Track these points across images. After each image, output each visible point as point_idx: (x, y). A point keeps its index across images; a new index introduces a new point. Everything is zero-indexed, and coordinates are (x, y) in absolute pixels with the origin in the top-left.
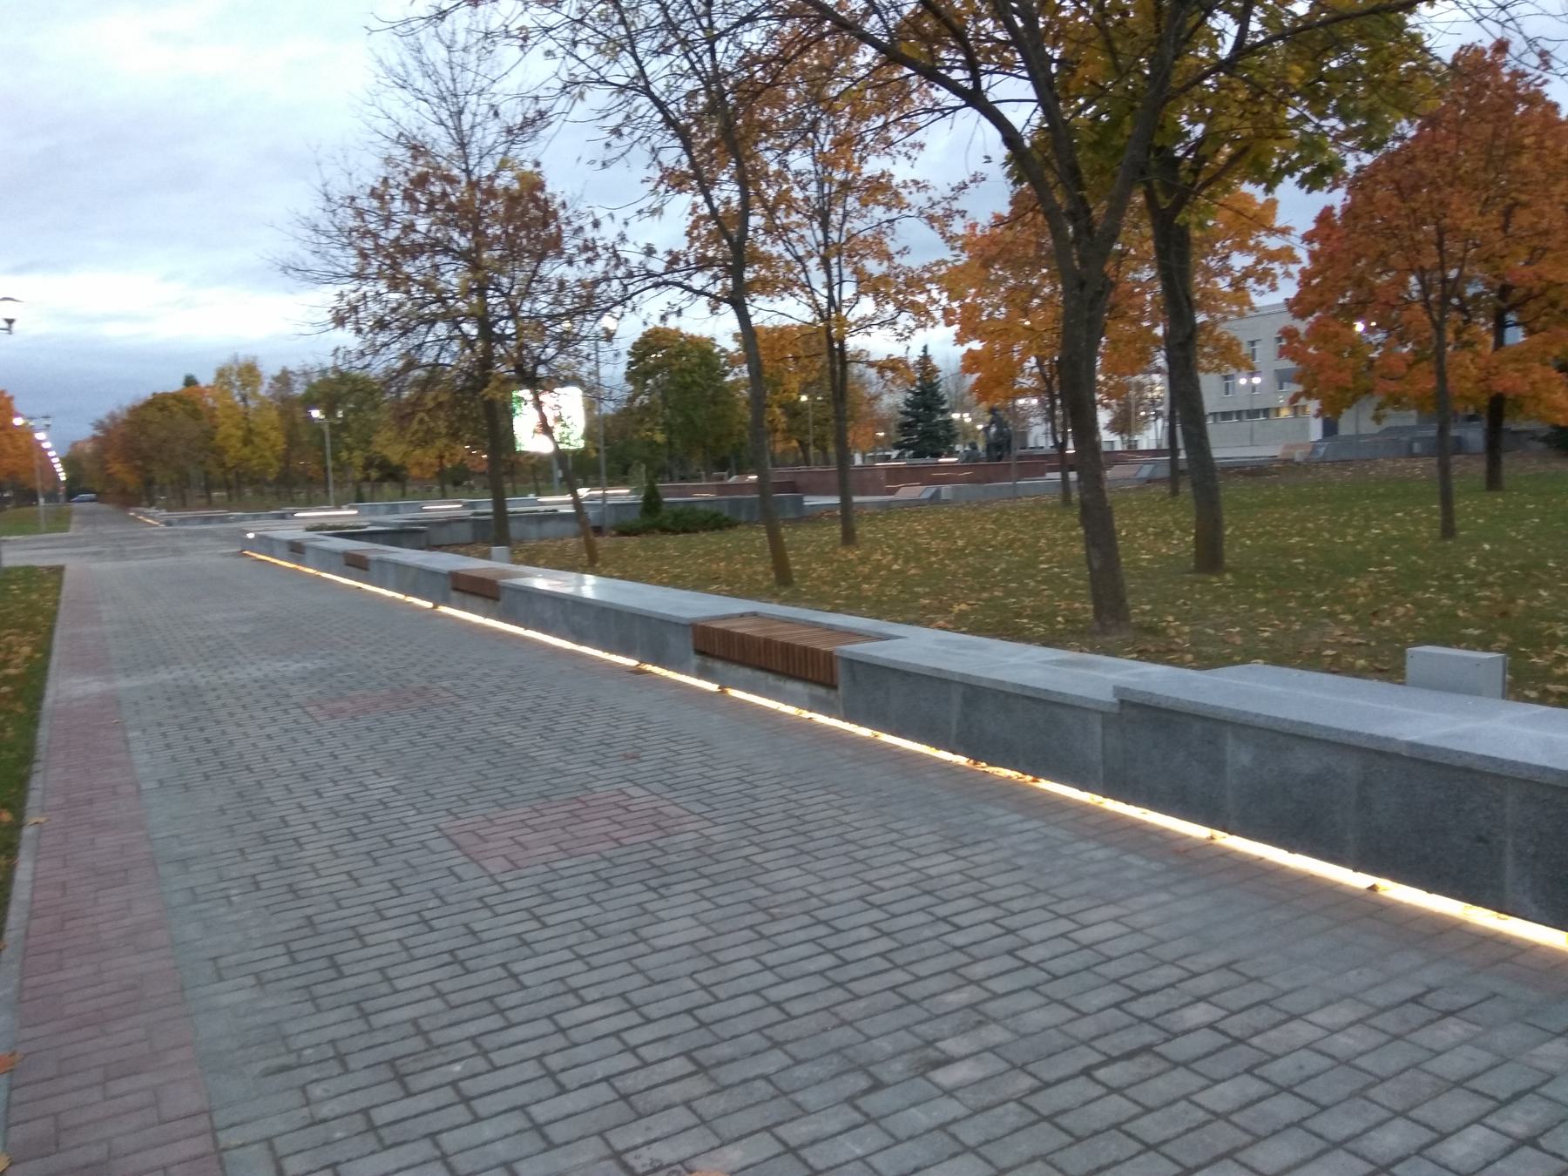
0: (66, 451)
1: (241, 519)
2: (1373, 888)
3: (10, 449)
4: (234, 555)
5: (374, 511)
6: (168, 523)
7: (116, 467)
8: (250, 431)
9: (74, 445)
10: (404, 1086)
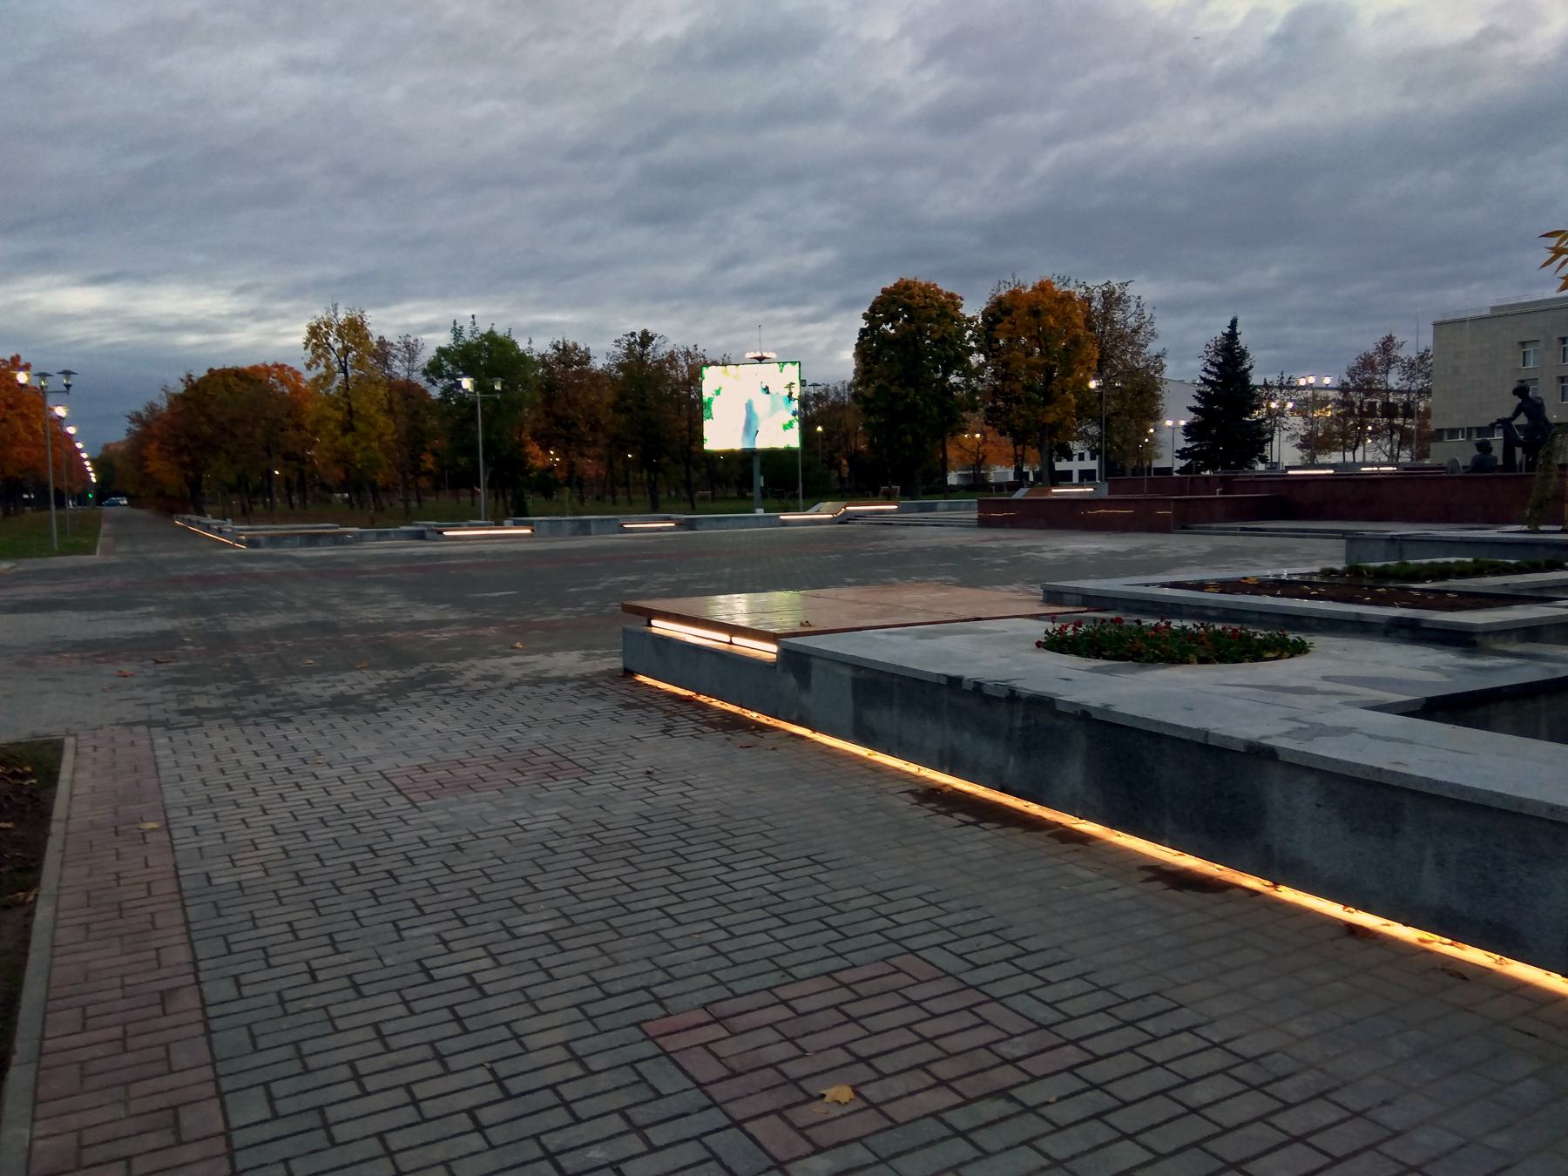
0: (98, 452)
1: (360, 538)
2: (1276, 885)
3: (23, 434)
4: (587, 683)
5: (555, 530)
6: (252, 543)
7: (156, 465)
8: (350, 412)
9: (106, 447)
10: (444, 1065)
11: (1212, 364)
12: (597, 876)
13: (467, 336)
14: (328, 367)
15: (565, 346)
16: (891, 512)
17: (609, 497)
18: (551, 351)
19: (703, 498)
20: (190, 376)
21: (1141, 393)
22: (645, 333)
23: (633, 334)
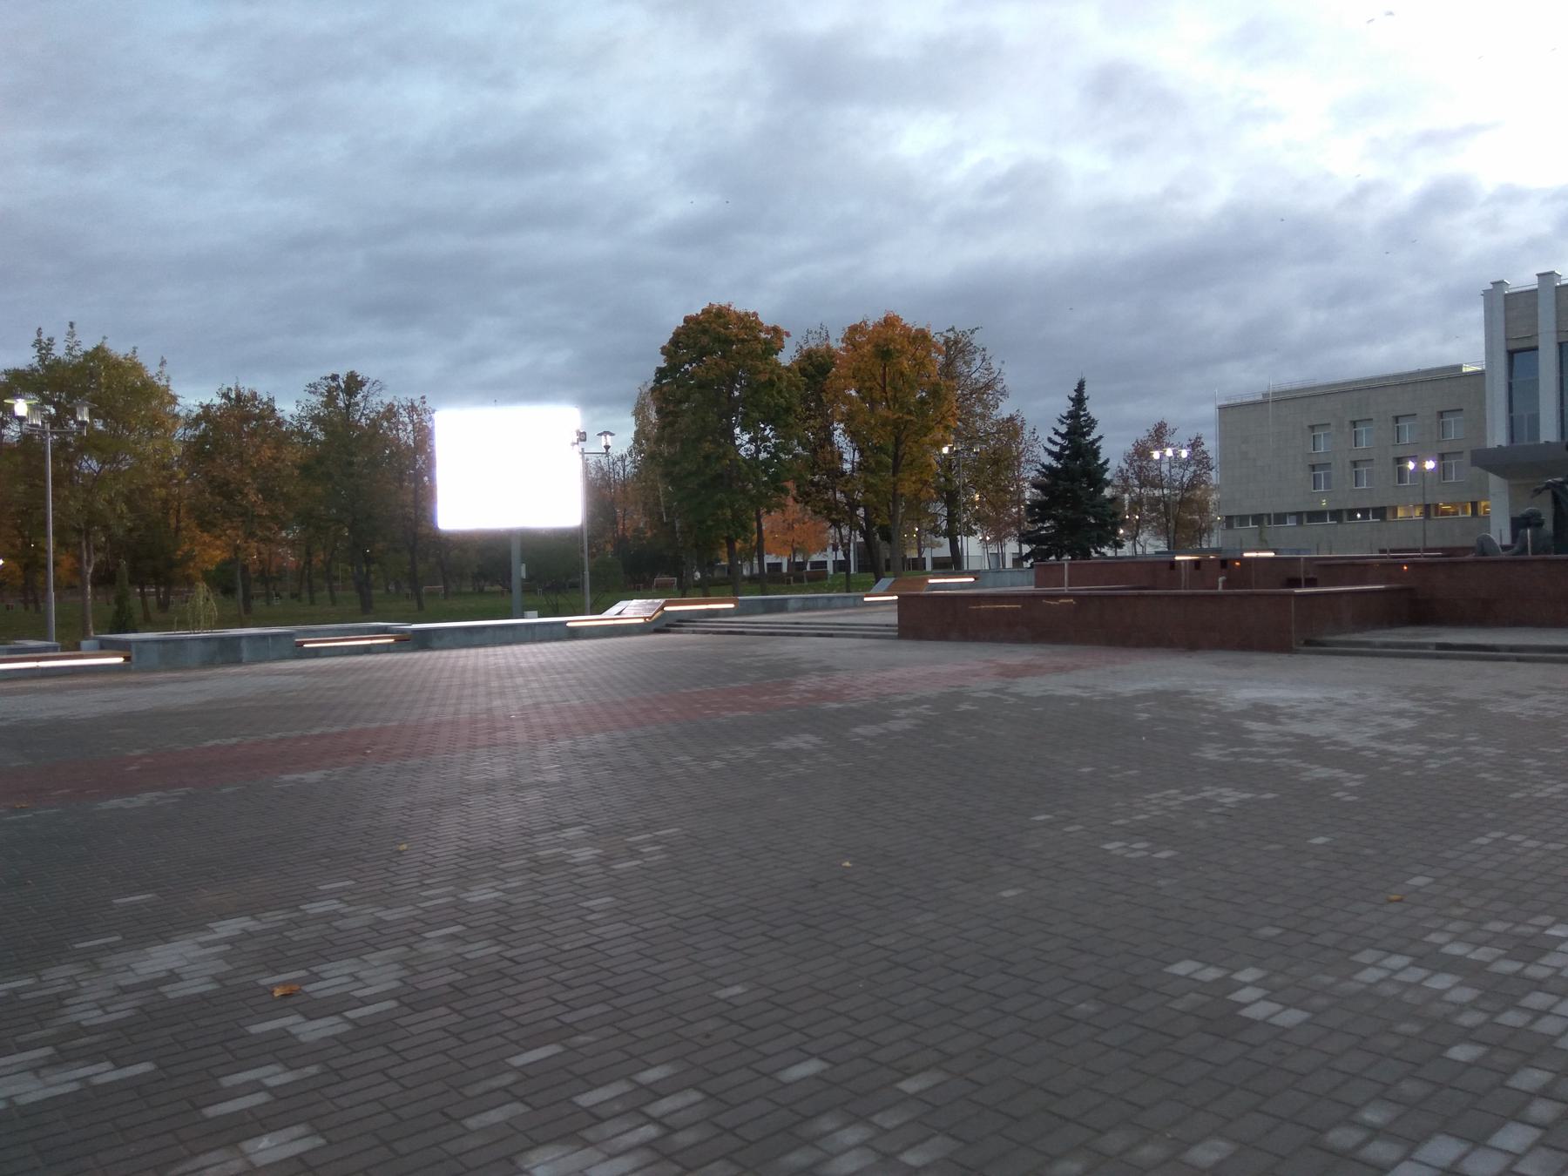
11: (1057, 433)
12: (345, 980)
13: (59, 351)
15: (239, 396)
16: (726, 612)
17: (305, 595)
18: (218, 401)
21: (996, 462)
22: (352, 377)
23: (335, 378)
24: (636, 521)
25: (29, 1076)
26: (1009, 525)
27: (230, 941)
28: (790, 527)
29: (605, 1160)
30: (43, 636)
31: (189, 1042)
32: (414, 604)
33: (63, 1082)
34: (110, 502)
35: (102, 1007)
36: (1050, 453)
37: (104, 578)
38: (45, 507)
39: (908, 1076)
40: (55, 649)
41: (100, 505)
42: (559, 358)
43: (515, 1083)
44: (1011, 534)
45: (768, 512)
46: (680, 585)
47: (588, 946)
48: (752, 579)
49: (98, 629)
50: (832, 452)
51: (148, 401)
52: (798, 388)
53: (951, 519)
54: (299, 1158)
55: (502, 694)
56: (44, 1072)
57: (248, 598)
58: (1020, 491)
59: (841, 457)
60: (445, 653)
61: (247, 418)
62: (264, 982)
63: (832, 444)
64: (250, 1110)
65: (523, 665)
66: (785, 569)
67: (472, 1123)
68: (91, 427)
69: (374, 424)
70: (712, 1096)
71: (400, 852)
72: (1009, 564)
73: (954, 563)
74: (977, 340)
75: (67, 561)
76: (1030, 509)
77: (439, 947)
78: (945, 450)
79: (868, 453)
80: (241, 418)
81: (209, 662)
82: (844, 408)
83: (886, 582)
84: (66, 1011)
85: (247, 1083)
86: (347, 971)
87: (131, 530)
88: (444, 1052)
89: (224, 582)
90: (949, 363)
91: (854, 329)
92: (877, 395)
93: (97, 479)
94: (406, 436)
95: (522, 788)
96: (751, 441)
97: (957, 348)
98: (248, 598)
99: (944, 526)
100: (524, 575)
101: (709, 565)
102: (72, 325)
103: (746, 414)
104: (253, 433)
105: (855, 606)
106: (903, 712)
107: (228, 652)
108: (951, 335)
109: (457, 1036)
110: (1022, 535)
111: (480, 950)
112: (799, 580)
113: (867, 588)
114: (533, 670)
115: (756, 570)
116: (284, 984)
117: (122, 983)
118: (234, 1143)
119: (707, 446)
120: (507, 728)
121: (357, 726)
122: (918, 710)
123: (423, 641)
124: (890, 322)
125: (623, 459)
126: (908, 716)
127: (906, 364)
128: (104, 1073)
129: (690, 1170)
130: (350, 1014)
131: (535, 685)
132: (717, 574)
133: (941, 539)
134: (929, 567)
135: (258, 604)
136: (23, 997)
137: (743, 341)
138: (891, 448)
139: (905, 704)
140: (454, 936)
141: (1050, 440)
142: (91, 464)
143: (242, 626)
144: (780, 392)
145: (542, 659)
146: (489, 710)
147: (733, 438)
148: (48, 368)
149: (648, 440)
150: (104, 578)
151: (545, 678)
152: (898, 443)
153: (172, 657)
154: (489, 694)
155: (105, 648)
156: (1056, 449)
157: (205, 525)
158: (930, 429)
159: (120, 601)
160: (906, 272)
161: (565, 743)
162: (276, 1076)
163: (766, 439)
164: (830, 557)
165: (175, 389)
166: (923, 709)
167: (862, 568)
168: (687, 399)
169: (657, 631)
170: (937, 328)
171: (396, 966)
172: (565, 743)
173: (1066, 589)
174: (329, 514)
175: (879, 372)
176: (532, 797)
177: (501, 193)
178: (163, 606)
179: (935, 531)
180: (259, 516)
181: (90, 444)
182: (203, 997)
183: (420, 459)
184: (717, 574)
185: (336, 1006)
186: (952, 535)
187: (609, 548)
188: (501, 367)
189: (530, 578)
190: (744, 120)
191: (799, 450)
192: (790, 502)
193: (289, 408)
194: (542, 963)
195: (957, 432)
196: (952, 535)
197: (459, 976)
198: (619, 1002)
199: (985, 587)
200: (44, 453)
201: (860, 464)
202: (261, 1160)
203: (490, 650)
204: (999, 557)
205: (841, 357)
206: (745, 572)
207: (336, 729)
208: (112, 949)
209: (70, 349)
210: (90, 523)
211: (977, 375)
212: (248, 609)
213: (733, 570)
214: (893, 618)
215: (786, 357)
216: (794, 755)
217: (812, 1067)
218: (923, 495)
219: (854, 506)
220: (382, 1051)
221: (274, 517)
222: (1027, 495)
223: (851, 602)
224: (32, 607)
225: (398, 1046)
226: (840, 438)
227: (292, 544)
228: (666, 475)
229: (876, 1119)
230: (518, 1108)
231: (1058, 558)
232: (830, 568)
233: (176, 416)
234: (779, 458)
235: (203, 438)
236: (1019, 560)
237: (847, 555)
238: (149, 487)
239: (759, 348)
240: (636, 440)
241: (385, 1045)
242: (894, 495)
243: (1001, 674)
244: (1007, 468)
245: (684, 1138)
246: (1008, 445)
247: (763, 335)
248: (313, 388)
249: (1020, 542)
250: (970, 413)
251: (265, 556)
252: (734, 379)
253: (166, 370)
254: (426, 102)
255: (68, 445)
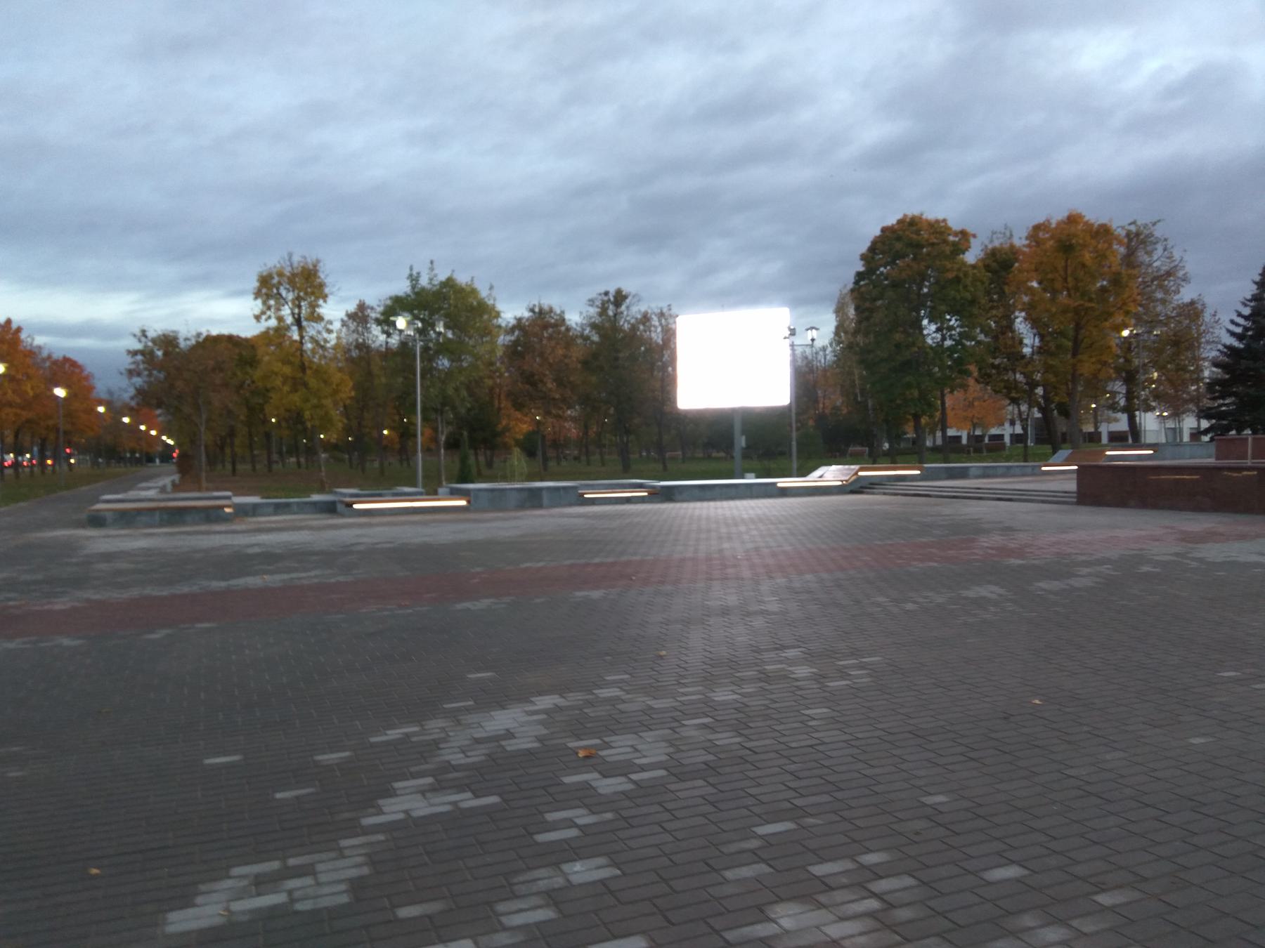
11: (1240, 315)
13: (424, 282)
14: (280, 319)
16: (913, 478)
17: (583, 458)
18: (527, 314)
19: (673, 458)
20: (144, 333)
23: (606, 293)
24: (834, 400)
25: (419, 796)
26: (1186, 402)
27: (546, 712)
28: (971, 405)
29: (835, 922)
30: (415, 485)
31: (528, 782)
32: (660, 467)
33: (441, 804)
34: (457, 390)
35: (463, 752)
36: (1233, 334)
37: (453, 444)
38: (415, 392)
39: (1104, 891)
40: (421, 494)
41: (450, 392)
42: (773, 268)
43: (759, 848)
44: (1189, 410)
45: (952, 392)
46: (870, 455)
47: (811, 746)
48: (935, 449)
49: (449, 480)
50: (1013, 338)
51: (481, 316)
52: (983, 283)
53: (1130, 396)
54: (603, 882)
55: (730, 538)
56: (428, 795)
57: (546, 460)
58: (1199, 370)
59: (1021, 342)
60: (685, 505)
61: (546, 326)
62: (571, 745)
63: (1013, 331)
64: (565, 841)
65: (745, 516)
66: (964, 441)
67: (729, 874)
68: (445, 335)
69: (634, 328)
70: (924, 883)
71: (661, 657)
72: (1186, 438)
73: (1133, 436)
74: (1158, 232)
75: (428, 431)
76: (1210, 386)
77: (694, 733)
78: (1125, 333)
79: (1048, 338)
80: (544, 324)
81: (521, 506)
82: (1026, 299)
83: (1064, 453)
84: (442, 752)
85: (565, 819)
86: (630, 743)
87: (469, 410)
88: (704, 815)
89: (529, 449)
90: (1131, 253)
91: (1037, 228)
92: (1058, 285)
93: (449, 374)
94: (657, 336)
95: (749, 614)
96: (938, 330)
97: (1138, 240)
98: (546, 460)
99: (1122, 402)
100: (743, 444)
101: (896, 437)
102: (432, 262)
103: (933, 308)
104: (550, 338)
105: (1033, 475)
106: (1085, 571)
107: (533, 500)
108: (1133, 228)
109: (712, 804)
110: (1201, 411)
111: (725, 739)
112: (978, 451)
113: (1045, 459)
114: (752, 521)
115: (939, 442)
116: (585, 748)
117: (476, 736)
118: (557, 864)
119: (898, 337)
120: (735, 566)
121: (624, 558)
122: (1098, 568)
123: (668, 495)
124: (1073, 219)
125: (824, 349)
126: (1090, 575)
127: (1088, 257)
128: (467, 801)
129: (908, 941)
130: (634, 777)
131: (755, 533)
132: (903, 445)
133: (1119, 415)
134: (1105, 440)
135: (552, 464)
136: (414, 739)
137: (933, 244)
138: (1071, 333)
139: (1088, 564)
140: (705, 726)
141: (1232, 322)
142: (444, 363)
143: (542, 480)
144: (965, 287)
145: (759, 512)
146: (721, 551)
147: (921, 328)
148: (417, 294)
149: (846, 333)
150: (453, 444)
151: (762, 527)
152: (1078, 327)
153: (497, 502)
154: (720, 538)
155: (455, 494)
156: (1239, 330)
157: (518, 406)
158: (1110, 315)
159: (464, 461)
160: (1087, 173)
161: (781, 581)
162: (584, 818)
163: (951, 328)
164: (1007, 431)
165: (500, 306)
166: (1105, 569)
167: (1039, 441)
168: (881, 297)
169: (853, 492)
170: (1119, 221)
171: (664, 744)
172: (781, 581)
173: (1249, 462)
174: (591, 397)
175: (1060, 264)
176: (758, 622)
177: (730, 137)
178: (490, 465)
179: (1113, 407)
180: (554, 399)
181: (445, 348)
182: (529, 752)
183: (666, 354)
184: (903, 445)
185: (624, 769)
186: (1130, 411)
187: (811, 423)
188: (726, 278)
189: (748, 447)
190: (936, 53)
191: (981, 337)
192: (971, 382)
193: (574, 318)
194: (773, 755)
195: (1138, 318)
196: (1130, 411)
197: (711, 757)
198: (839, 795)
199: (1164, 459)
200: (415, 355)
201: (1040, 348)
202: (576, 879)
203: (718, 504)
204: (1176, 432)
205: (1024, 253)
206: (929, 443)
207: (610, 560)
208: (468, 710)
209: (431, 279)
210: (443, 405)
211: (1158, 261)
212: (545, 469)
213: (917, 442)
214: (1072, 486)
215: (972, 256)
216: (980, 602)
217: (1012, 872)
218: (1102, 375)
219: (1033, 385)
220: (657, 808)
221: (564, 400)
222: (1206, 373)
223: (1029, 470)
224: (405, 464)
225: (670, 806)
226: (1021, 325)
227: (574, 419)
228: (862, 362)
229: (1075, 923)
230: (763, 868)
231: (1239, 432)
232: (1007, 439)
233: (499, 327)
234: (963, 345)
235: (516, 343)
236: (1196, 434)
237: (1025, 429)
238: (481, 378)
239: (948, 249)
240: (837, 333)
241: (660, 804)
242: (1073, 375)
243: (1183, 540)
244: (1187, 349)
245: (904, 914)
246: (1189, 327)
247: (951, 238)
248: (591, 302)
249: (1199, 418)
250: (1151, 299)
251: (557, 429)
252: (924, 277)
253: (494, 293)
254: (674, 72)
255: (429, 349)
